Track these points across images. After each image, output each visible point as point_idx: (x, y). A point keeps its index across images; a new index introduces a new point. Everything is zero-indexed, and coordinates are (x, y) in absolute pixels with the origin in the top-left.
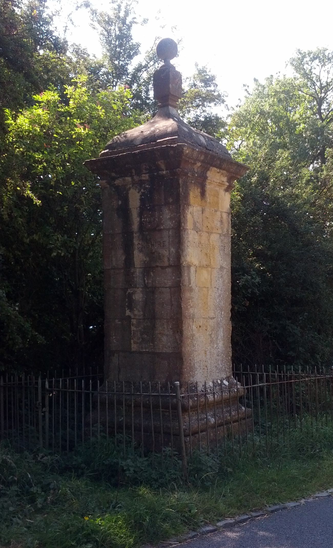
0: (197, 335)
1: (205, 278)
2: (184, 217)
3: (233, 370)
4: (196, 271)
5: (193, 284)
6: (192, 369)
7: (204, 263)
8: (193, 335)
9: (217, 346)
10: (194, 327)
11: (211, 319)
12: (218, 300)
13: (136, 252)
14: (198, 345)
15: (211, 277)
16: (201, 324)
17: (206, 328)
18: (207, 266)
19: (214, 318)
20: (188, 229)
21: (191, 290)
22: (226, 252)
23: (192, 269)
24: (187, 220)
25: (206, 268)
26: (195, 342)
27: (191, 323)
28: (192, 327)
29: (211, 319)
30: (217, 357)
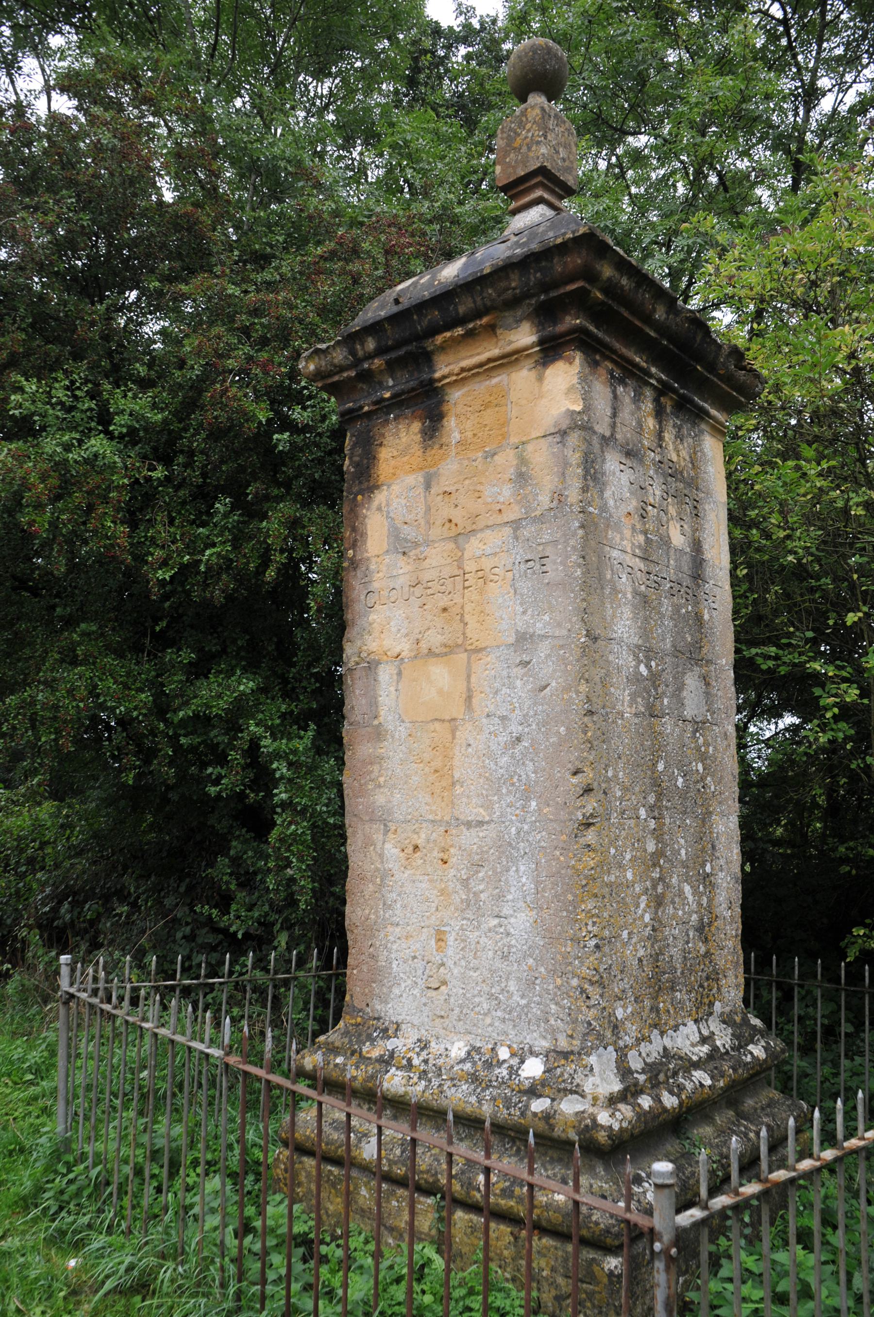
0: (402, 876)
1: (440, 692)
2: (354, 529)
3: (747, 970)
4: (400, 674)
5: (386, 716)
6: (377, 975)
7: (434, 639)
8: (387, 874)
9: (843, 76)
10: (391, 850)
11: (469, 825)
12: (504, 760)
13: (483, 1182)
14: (404, 907)
15: (469, 682)
16: (420, 842)
17: (441, 855)
18: (449, 650)
19: (481, 823)
20: (368, 559)
21: (379, 734)
22: (555, 571)
23: (385, 674)
24: (364, 535)
25: (446, 654)
26: (394, 895)
27: (378, 837)
28: (382, 849)
29: (469, 825)
30: (498, 964)
